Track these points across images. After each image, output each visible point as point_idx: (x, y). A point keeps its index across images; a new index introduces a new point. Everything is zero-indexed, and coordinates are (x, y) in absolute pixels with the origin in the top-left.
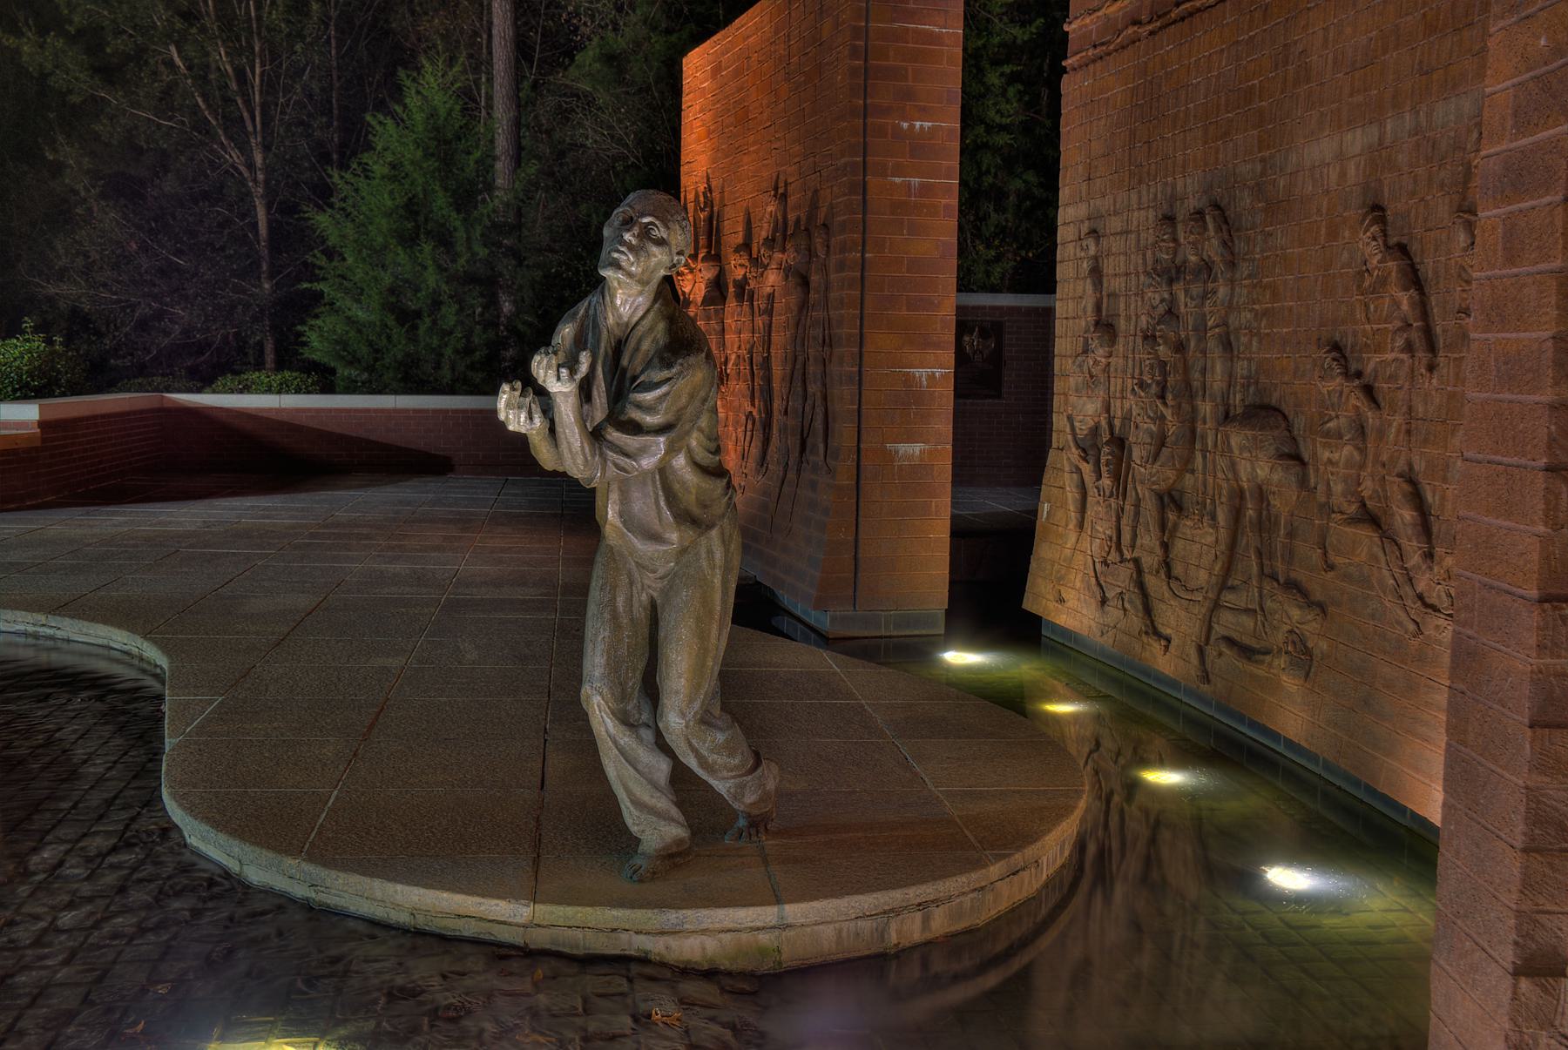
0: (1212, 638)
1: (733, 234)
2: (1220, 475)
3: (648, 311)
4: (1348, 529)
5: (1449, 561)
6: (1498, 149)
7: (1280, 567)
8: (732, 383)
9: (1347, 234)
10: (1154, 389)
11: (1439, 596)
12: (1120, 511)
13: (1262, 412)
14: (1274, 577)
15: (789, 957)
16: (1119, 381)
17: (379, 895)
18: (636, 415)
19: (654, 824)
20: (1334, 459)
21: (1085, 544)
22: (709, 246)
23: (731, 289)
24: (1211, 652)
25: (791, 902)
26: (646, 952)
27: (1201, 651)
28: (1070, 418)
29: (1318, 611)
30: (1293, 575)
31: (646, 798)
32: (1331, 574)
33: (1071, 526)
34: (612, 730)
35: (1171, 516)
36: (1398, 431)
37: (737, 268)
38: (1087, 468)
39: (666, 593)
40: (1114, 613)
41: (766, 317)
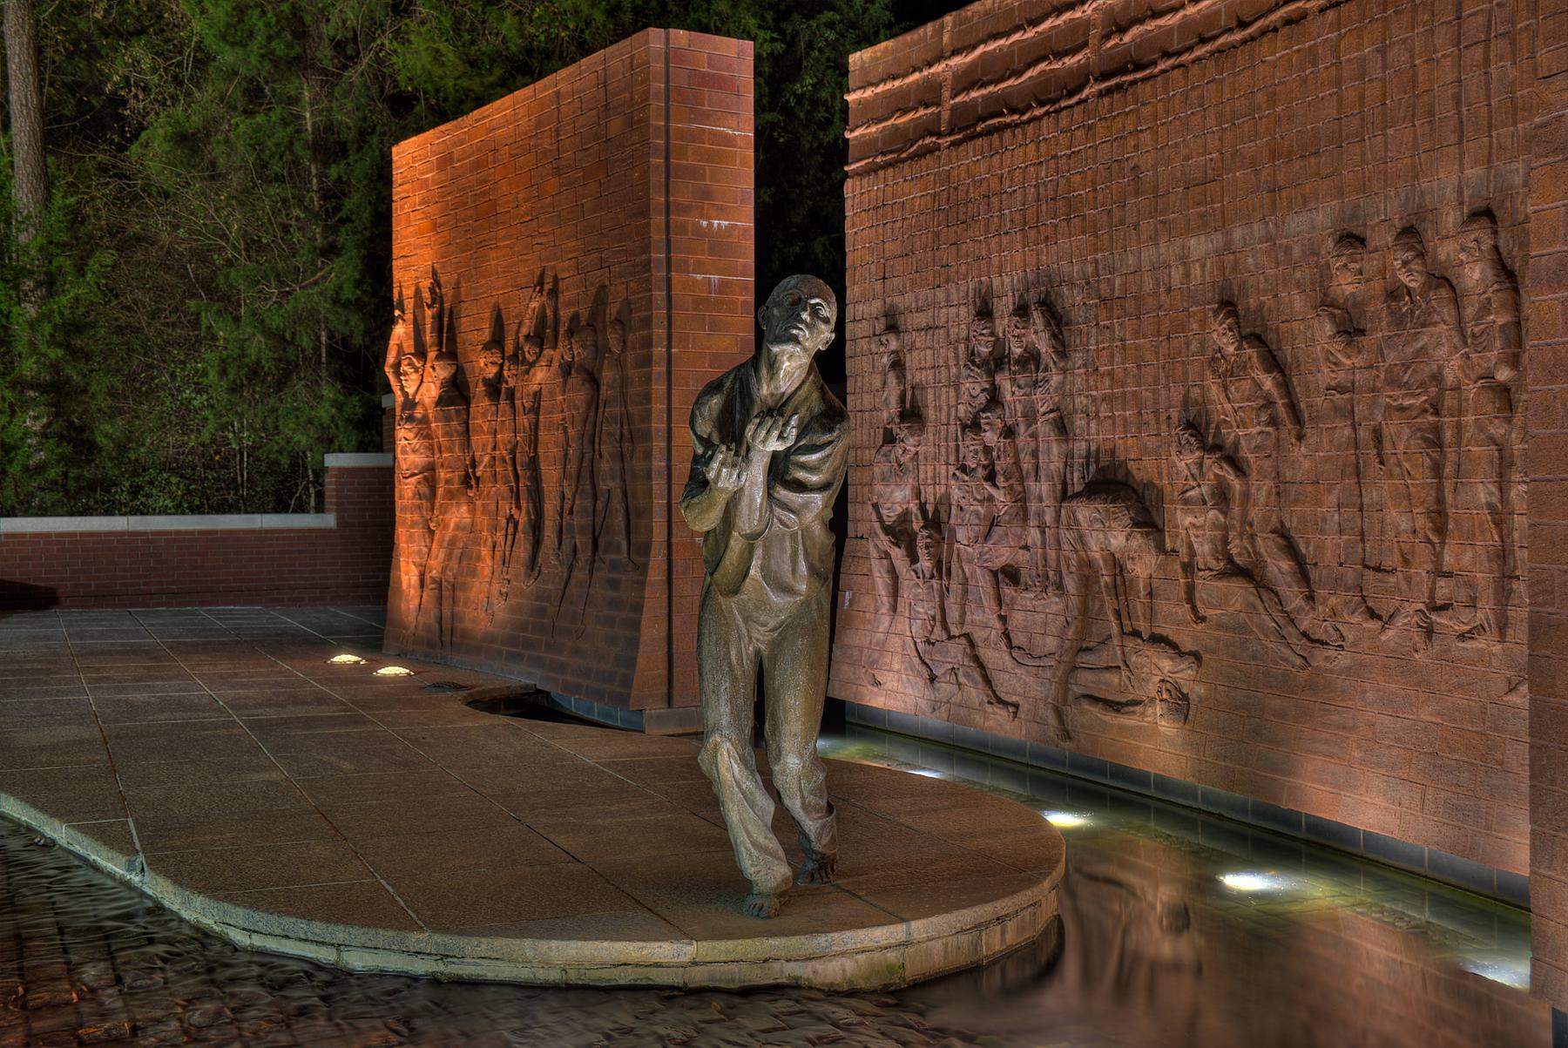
0: (1070, 698)
1: (474, 330)
2: (1066, 547)
3: (803, 382)
4: (1219, 584)
5: (1333, 600)
6: (1550, 250)
7: (1142, 626)
8: (486, 487)
9: (1195, 326)
10: (981, 473)
11: (1326, 632)
12: (944, 593)
13: (1109, 483)
14: (1136, 634)
15: (910, 973)
16: (930, 469)
17: (530, 954)
18: (801, 475)
19: (762, 863)
20: (1192, 526)
21: (902, 625)
22: (440, 344)
23: (481, 388)
24: (1071, 712)
25: (915, 919)
26: (796, 979)
27: (1059, 713)
28: (876, 506)
29: (1192, 659)
30: (1157, 631)
31: (761, 840)
32: (1201, 627)
33: (884, 610)
34: (737, 776)
35: (1008, 591)
36: (1269, 494)
37: (483, 365)
38: (898, 554)
39: (776, 646)
40: (946, 688)
41: (532, 416)
